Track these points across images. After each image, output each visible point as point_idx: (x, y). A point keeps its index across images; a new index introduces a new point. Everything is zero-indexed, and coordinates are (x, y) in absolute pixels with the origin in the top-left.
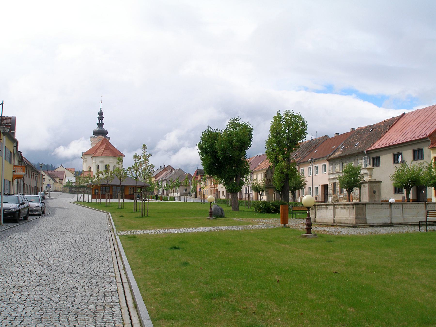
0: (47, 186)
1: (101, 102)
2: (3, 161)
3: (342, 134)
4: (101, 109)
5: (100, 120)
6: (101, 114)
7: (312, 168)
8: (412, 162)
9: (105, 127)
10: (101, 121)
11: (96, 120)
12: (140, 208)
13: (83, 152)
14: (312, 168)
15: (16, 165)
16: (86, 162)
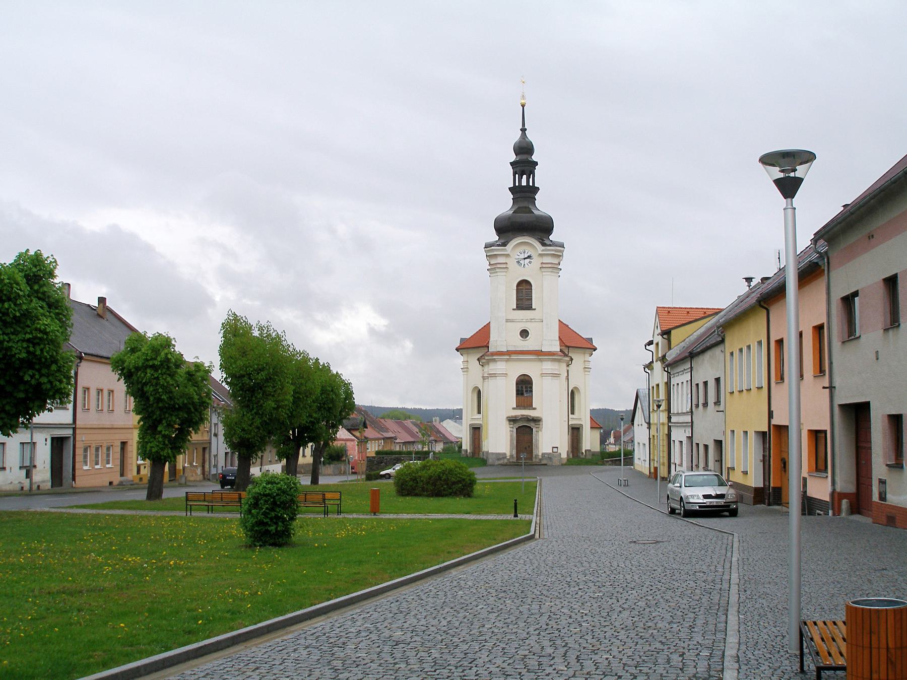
1: (523, 106)
2: (727, 396)
4: (523, 130)
5: (525, 177)
6: (524, 150)
7: (829, 328)
9: (543, 205)
11: (507, 178)
12: (887, 644)
13: (663, 313)
14: (829, 328)
15: (682, 410)
16: (467, 371)
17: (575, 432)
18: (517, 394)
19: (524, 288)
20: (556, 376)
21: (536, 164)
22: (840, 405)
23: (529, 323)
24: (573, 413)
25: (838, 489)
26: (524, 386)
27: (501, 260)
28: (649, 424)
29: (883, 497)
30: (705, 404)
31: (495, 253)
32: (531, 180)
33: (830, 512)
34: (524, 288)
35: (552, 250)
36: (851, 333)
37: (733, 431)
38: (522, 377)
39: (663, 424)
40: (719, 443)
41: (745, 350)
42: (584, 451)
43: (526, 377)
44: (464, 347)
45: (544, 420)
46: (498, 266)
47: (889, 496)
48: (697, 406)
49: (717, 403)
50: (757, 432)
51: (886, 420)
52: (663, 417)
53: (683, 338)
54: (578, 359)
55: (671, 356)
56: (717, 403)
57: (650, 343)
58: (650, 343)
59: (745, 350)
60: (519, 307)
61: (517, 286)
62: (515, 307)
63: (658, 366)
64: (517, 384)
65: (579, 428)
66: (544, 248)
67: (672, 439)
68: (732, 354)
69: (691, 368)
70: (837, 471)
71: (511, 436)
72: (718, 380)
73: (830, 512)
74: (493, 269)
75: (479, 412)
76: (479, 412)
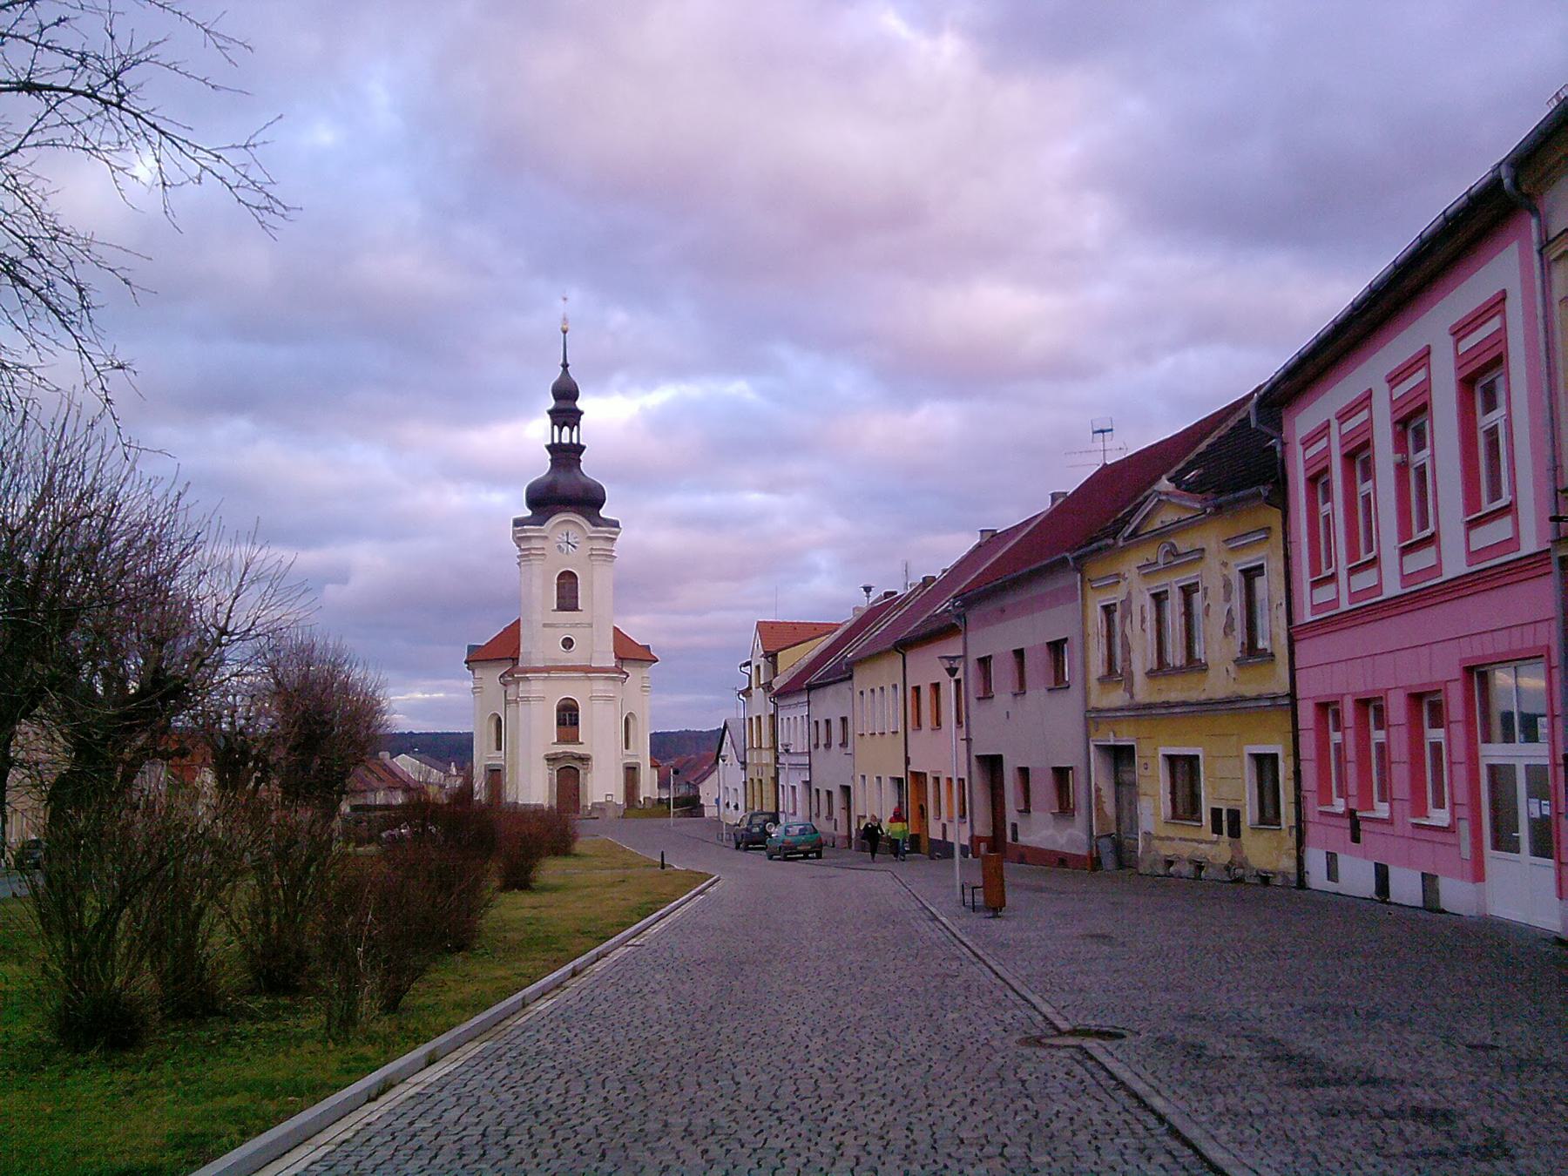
0: (1269, 651)
3: (454, 734)
4: (565, 366)
5: (566, 429)
8: (1349, 579)
10: (572, 430)
13: (765, 629)
17: (631, 771)
18: (559, 724)
19: (567, 581)
20: (610, 699)
21: (582, 413)
22: (978, 757)
23: (575, 629)
24: (627, 748)
25: (976, 833)
26: (568, 716)
27: (536, 544)
28: (744, 763)
29: (1015, 839)
30: (828, 745)
31: (528, 534)
32: (575, 433)
33: (970, 855)
34: (567, 581)
35: (606, 532)
36: (986, 695)
37: (863, 777)
38: (564, 702)
39: (767, 765)
40: (846, 790)
41: (877, 690)
42: (642, 799)
43: (570, 702)
44: (478, 658)
45: (594, 758)
46: (533, 552)
47: (1020, 838)
48: (817, 746)
49: (844, 744)
50: (892, 778)
51: (1016, 771)
52: (767, 757)
53: (793, 660)
54: (635, 674)
55: (778, 684)
56: (844, 744)
57: (749, 664)
58: (749, 664)
59: (877, 690)
60: (562, 607)
61: (559, 578)
62: (555, 607)
63: (758, 694)
64: (558, 711)
65: (635, 768)
66: (594, 528)
67: (781, 783)
68: (862, 693)
69: (809, 701)
70: (975, 816)
71: (550, 780)
72: (844, 720)
73: (970, 855)
74: (525, 556)
75: (499, 748)
76: (499, 748)
